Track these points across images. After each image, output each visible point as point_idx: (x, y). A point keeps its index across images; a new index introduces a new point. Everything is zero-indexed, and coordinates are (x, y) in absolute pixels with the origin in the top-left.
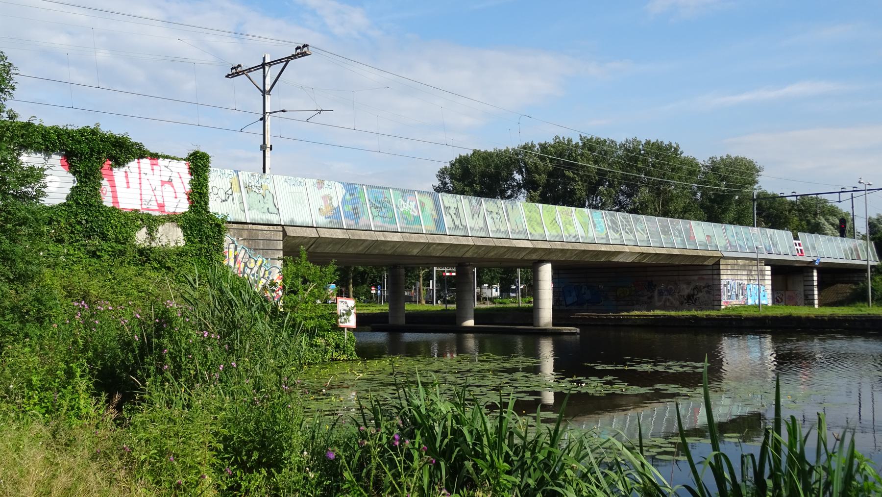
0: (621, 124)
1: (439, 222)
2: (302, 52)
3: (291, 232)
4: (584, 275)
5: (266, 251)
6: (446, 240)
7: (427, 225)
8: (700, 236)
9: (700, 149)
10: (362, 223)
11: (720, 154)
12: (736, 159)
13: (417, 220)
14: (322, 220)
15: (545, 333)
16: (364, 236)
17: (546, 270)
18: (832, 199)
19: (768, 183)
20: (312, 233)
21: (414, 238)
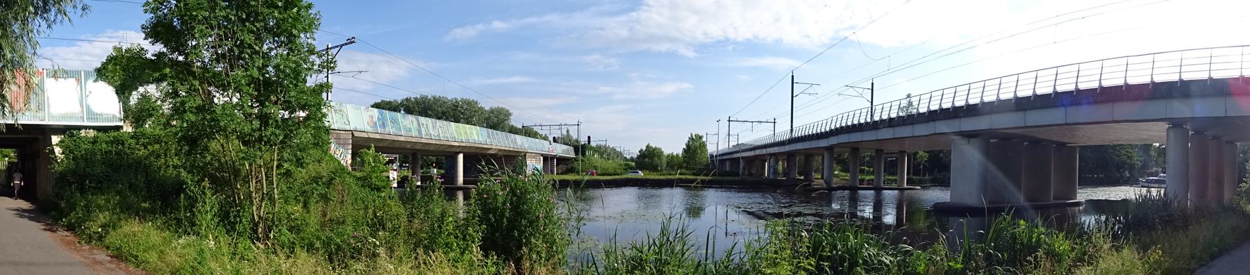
0: (451, 92)
1: (420, 131)
2: (351, 41)
3: (356, 134)
4: (476, 157)
5: (344, 145)
6: (424, 141)
7: (415, 133)
8: (521, 143)
9: (487, 104)
10: (387, 130)
11: (495, 106)
12: (492, 111)
13: (410, 130)
14: (368, 128)
15: (460, 188)
16: (388, 137)
17: (461, 157)
18: (535, 129)
19: (516, 122)
20: (365, 135)
21: (410, 139)
